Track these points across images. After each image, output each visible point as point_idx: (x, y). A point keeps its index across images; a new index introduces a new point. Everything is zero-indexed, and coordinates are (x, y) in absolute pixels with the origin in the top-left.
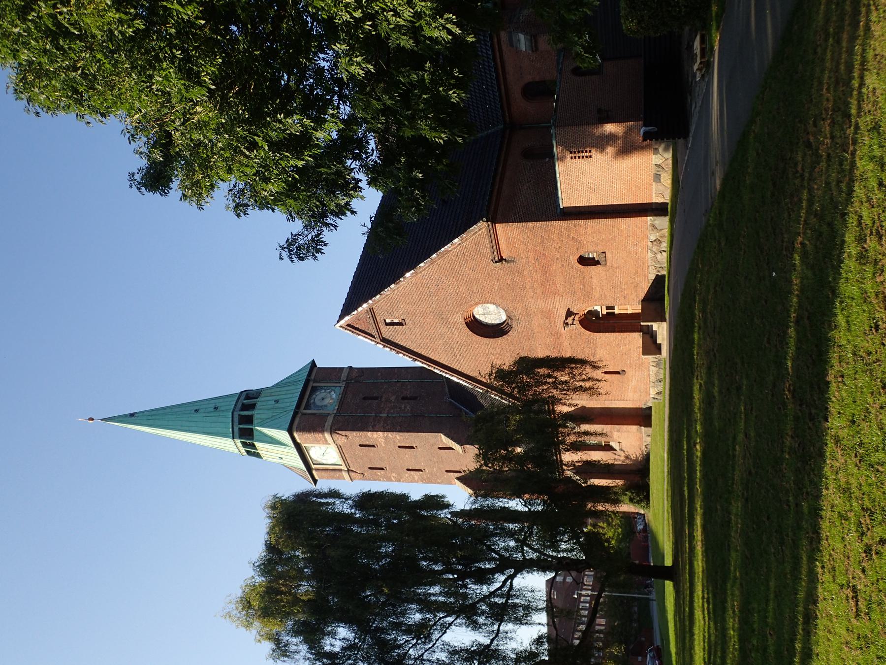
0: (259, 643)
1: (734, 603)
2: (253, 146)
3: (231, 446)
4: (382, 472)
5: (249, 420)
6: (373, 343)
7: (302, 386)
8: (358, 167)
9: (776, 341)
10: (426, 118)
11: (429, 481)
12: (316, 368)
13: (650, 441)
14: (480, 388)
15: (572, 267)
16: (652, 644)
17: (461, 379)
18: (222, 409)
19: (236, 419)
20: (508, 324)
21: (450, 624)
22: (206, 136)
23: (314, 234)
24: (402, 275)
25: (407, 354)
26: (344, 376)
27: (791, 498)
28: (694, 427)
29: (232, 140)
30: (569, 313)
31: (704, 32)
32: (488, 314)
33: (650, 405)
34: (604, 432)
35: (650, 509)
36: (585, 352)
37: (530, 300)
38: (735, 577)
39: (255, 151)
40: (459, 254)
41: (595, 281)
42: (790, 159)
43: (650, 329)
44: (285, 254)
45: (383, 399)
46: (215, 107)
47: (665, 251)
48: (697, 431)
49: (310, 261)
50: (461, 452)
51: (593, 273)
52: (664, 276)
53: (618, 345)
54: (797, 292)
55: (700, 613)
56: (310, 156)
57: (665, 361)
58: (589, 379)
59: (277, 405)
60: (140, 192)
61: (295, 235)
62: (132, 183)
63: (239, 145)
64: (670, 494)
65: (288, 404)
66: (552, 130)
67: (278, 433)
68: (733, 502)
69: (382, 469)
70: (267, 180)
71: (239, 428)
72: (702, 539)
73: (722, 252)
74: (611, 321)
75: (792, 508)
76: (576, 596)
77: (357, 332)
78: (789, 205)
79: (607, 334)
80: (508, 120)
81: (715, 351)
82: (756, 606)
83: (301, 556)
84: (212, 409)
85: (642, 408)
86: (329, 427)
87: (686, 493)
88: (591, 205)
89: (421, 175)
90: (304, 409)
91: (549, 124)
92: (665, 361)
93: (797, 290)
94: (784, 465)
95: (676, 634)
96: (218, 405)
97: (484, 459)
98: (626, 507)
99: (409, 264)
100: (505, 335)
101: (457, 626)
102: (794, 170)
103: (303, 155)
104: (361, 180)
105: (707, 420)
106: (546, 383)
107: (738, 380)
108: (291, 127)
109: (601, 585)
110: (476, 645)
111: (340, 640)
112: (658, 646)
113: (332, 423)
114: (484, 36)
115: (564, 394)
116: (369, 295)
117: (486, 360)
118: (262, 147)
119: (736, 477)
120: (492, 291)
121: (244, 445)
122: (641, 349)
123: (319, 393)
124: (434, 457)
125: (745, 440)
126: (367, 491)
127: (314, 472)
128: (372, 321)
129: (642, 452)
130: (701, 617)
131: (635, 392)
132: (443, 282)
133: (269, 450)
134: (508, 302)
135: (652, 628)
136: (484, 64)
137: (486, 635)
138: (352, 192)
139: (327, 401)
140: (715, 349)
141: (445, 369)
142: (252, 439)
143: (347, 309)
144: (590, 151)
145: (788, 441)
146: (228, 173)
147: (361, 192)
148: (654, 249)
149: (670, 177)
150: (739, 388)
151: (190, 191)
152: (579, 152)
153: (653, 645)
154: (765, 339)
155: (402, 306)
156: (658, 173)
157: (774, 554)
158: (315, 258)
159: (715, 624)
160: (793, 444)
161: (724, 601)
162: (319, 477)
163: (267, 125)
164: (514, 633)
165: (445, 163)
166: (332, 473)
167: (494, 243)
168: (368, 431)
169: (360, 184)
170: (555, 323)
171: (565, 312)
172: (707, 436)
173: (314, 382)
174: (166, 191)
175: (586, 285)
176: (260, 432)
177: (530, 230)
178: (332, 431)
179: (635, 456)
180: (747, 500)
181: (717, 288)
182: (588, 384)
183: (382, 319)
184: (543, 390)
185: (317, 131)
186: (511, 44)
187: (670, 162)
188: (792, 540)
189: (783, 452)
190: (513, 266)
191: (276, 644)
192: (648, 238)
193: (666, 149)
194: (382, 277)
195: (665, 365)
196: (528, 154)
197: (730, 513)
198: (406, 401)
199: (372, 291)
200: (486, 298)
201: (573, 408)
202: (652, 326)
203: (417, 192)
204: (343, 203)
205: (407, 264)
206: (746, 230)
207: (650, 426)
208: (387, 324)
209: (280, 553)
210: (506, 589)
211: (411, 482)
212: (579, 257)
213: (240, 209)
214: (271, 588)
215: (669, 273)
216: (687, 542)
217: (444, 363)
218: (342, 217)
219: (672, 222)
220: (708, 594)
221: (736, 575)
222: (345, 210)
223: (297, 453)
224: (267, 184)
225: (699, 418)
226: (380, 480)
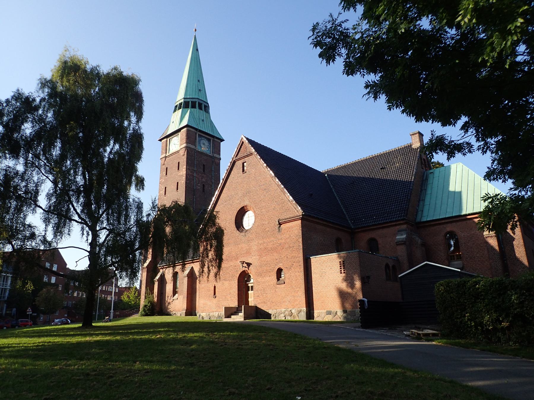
3: (180, 97)
4: (165, 174)
5: (194, 106)
6: (233, 156)
12: (220, 142)
18: (200, 94)
19: (194, 100)
26: (215, 155)
30: (249, 265)
31: (440, 335)
36: (227, 274)
40: (283, 201)
45: (203, 175)
47: (285, 318)
52: (270, 318)
53: (230, 293)
58: (209, 271)
64: (139, 323)
65: (201, 126)
69: (166, 174)
71: (189, 102)
77: (239, 147)
80: (357, 230)
84: (199, 89)
85: (196, 310)
86: (189, 146)
96: (202, 92)
105: (175, 341)
114: (404, 216)
117: (223, 219)
121: (181, 104)
127: (165, 139)
128: (245, 155)
129: (172, 312)
131: (204, 304)
134: (255, 229)
136: (387, 217)
140: (226, 346)
142: (183, 108)
144: (344, 273)
150: (192, 365)
154: (233, 390)
155: (253, 171)
156: (332, 313)
166: (165, 148)
168: (186, 166)
173: (213, 140)
176: (187, 112)
182: (206, 269)
186: (400, 231)
187: (339, 320)
192: (293, 308)
193: (345, 318)
198: (202, 187)
200: (258, 217)
207: (186, 315)
208: (243, 164)
211: (159, 190)
215: (273, 321)
217: (221, 197)
226: (160, 173)
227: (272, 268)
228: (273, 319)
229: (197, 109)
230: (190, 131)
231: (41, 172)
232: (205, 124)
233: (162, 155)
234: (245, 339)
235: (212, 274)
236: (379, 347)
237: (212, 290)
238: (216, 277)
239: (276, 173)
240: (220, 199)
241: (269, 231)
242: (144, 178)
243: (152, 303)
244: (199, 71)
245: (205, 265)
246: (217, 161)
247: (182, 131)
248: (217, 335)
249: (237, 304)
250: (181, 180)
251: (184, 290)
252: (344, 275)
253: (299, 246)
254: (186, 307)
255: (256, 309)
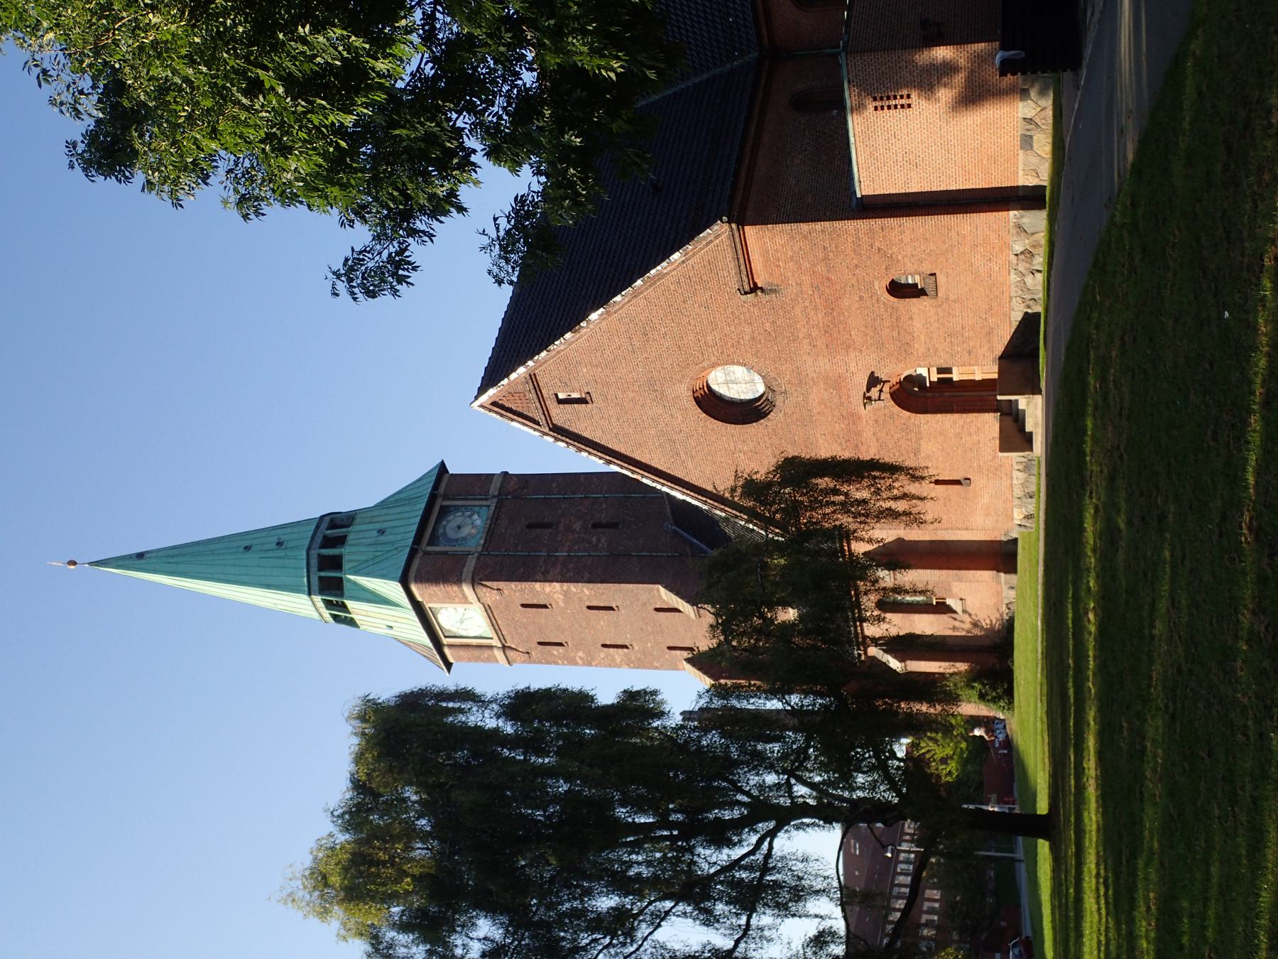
0: (344, 943)
1: (1148, 899)
2: (255, 88)
4: (561, 649)
5: (336, 563)
6: (537, 434)
7: (423, 506)
8: (468, 126)
9: (1228, 436)
10: (585, 33)
11: (640, 664)
12: (447, 475)
13: (1014, 596)
14: (721, 510)
15: (878, 301)
16: (1018, 934)
17: (688, 495)
18: (290, 544)
19: (314, 562)
20: (767, 399)
21: (667, 913)
22: (176, 70)
23: (392, 250)
24: (584, 317)
25: (595, 452)
26: (494, 489)
27: (1250, 723)
28: (1085, 581)
29: (217, 77)
30: (873, 381)
32: (733, 382)
33: (1014, 535)
34: (930, 588)
35: (1013, 710)
37: (805, 357)
38: (1151, 848)
39: (261, 97)
41: (918, 325)
42: (1258, 101)
43: (1013, 406)
44: (342, 286)
45: (561, 528)
46: (183, 13)
47: (1039, 271)
48: (1089, 588)
49: (385, 299)
50: (692, 616)
51: (914, 310)
52: (1038, 315)
53: (958, 436)
54: (1267, 349)
55: (1093, 901)
56: (366, 106)
57: (1039, 462)
58: (905, 496)
59: (382, 538)
60: (87, 176)
61: (360, 252)
62: (74, 159)
63: (228, 85)
64: (1045, 691)
65: (399, 537)
66: (842, 60)
67: (382, 584)
68: (1149, 717)
69: (561, 644)
70: (285, 151)
72: (1096, 775)
73: (1136, 273)
74: (946, 394)
75: (1252, 739)
76: (889, 855)
78: (1255, 188)
79: (939, 415)
80: (766, 41)
81: (1122, 450)
82: (1185, 904)
83: (414, 798)
84: (274, 546)
85: (1000, 541)
86: (470, 575)
87: (1071, 692)
88: (911, 191)
89: (578, 140)
90: (428, 545)
91: (836, 50)
92: (1039, 462)
93: (1268, 345)
94: (1239, 663)
95: (1054, 928)
96: (283, 538)
97: (724, 632)
98: (971, 707)
99: (595, 298)
100: (763, 418)
101: (678, 916)
102: (1265, 122)
103: (354, 105)
104: (474, 151)
105: (1107, 572)
106: (828, 504)
107: (1160, 503)
108: (324, 51)
109: (926, 841)
110: (709, 951)
111: (479, 940)
112: (1027, 937)
113: (475, 568)
115: (861, 523)
116: (529, 351)
117: (730, 462)
118: (272, 89)
119: (1154, 675)
120: (739, 342)
121: (329, 604)
122: (998, 442)
123: (452, 516)
124: (647, 624)
125: (1171, 610)
126: (522, 687)
127: (446, 650)
128: (535, 396)
129: (1001, 615)
130: (1095, 907)
131: (988, 515)
132: (654, 328)
133: (370, 614)
135: (1020, 906)
137: (728, 932)
138: (457, 172)
139: (465, 531)
140: (1122, 447)
141: (660, 478)
142: (342, 595)
143: (492, 377)
144: (909, 97)
145: (1246, 618)
146: (211, 138)
147: (476, 172)
148: (1021, 268)
149: (1050, 140)
150: (1162, 518)
151: (156, 174)
152: (888, 98)
153: (1021, 935)
154: (1209, 432)
156: (1029, 133)
157: (1219, 818)
158: (395, 292)
159: (1118, 923)
160: (1256, 626)
161: (1132, 888)
162: (455, 659)
163: (277, 47)
164: (774, 931)
165: (625, 118)
166: (476, 652)
167: (742, 261)
168: (536, 581)
169: (473, 158)
170: (849, 397)
171: (866, 379)
172: (1107, 599)
174: (127, 174)
175: (902, 332)
176: (355, 583)
177: (805, 237)
178: (474, 583)
179: (988, 622)
180: (1173, 717)
181: (1126, 338)
182: (901, 506)
183: (552, 392)
184: (824, 514)
185: (376, 59)
187: (1049, 113)
188: (1251, 796)
189: (1237, 637)
190: (775, 299)
191: (372, 944)
192: (1010, 248)
193: (1042, 93)
194: (550, 321)
195: (1039, 468)
196: (801, 103)
197: (1143, 738)
198: (599, 530)
199: (534, 345)
200: (729, 356)
201: (876, 546)
202: (1017, 401)
203: (572, 170)
204: (441, 192)
205: (592, 297)
206: (1177, 233)
208: (560, 402)
209: (376, 795)
210: (759, 857)
211: (610, 666)
212: (890, 283)
213: (248, 204)
214: (361, 854)
215: (1047, 310)
216: (1072, 777)
218: (442, 218)
219: (1052, 220)
220: (1106, 869)
221: (1152, 846)
222: (447, 207)
223: (416, 619)
224: (287, 158)
225: (1093, 565)
226: (556, 663)
227: (886, 311)
228: (1039, 308)
229: (346, 551)
230: (418, 571)
231: (634, 952)
232: (391, 524)
233: (497, 661)
234: (1105, 399)
235: (913, 488)
236: (1135, 37)
237: (947, 490)
238: (923, 478)
239: (593, 302)
240: (669, 471)
241: (774, 322)
242: (625, 691)
243: (971, 678)
244: (213, 547)
245: (889, 509)
246: (512, 486)
247: (419, 599)
248: (1093, 465)
249: (992, 415)
250: (580, 599)
251: (936, 579)
252: (914, 95)
253: (823, 231)
254: (991, 572)
255: (1007, 358)
